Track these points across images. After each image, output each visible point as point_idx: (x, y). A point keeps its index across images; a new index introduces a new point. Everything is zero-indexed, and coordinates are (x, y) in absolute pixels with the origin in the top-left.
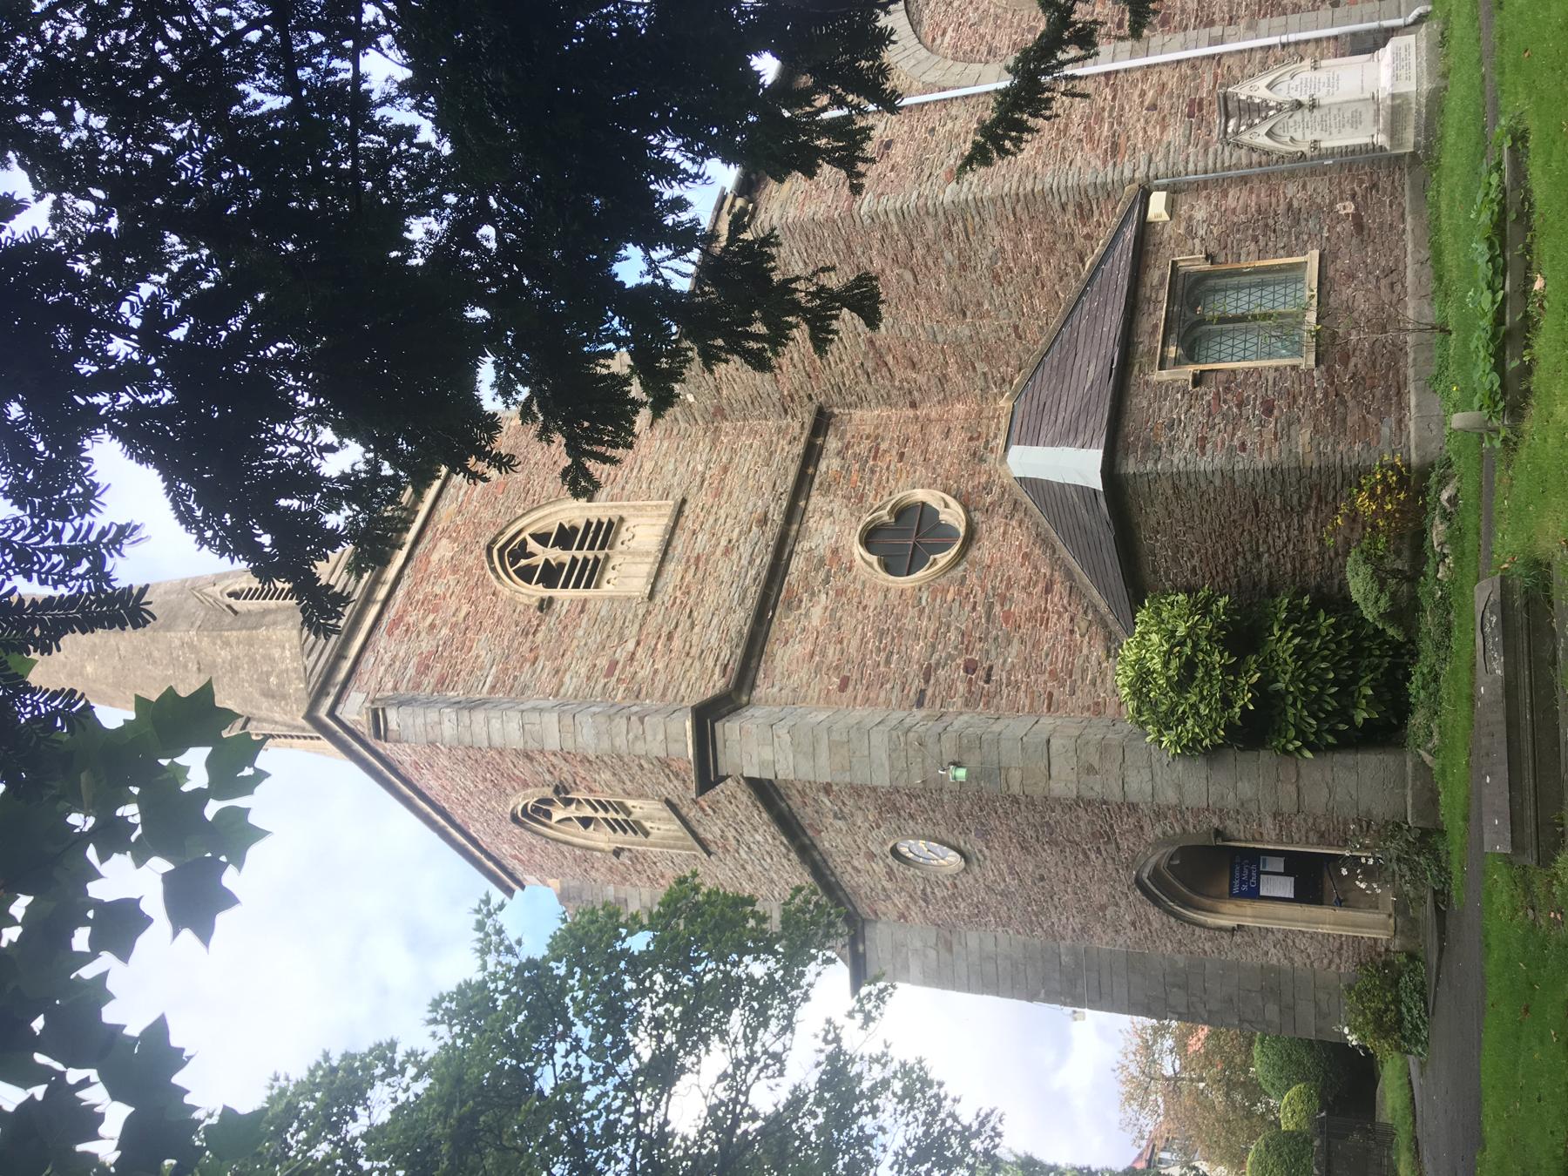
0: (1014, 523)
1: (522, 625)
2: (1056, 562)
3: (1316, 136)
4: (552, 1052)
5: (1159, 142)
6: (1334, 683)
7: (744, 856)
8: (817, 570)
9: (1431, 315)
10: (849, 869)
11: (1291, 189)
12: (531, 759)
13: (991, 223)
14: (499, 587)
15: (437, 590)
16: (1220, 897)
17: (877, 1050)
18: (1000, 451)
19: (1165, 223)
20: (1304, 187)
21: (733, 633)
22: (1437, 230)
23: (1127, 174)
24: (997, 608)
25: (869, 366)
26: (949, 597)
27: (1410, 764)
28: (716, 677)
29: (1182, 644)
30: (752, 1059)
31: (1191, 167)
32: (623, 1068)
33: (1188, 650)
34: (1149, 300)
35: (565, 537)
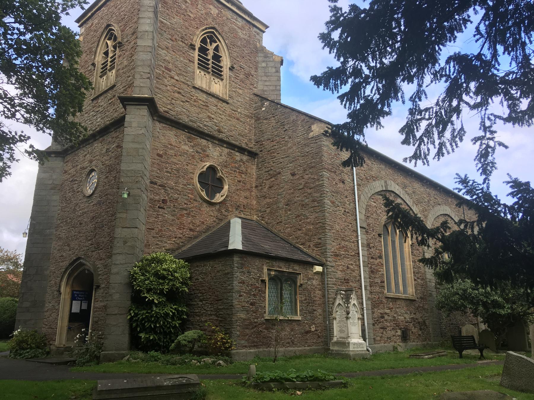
0: (215, 219)
1: (185, 37)
2: (201, 233)
3: (338, 319)
4: (20, 23)
5: (337, 269)
6: (155, 326)
7: (91, 114)
8: (201, 149)
9: (279, 355)
10: (85, 153)
11: (320, 311)
12: (133, 34)
13: (317, 215)
14: (200, 30)
15: (199, 6)
16: (72, 286)
17: (15, 156)
18: (239, 216)
19: (313, 271)
20: (320, 315)
21: (180, 116)
22: (305, 357)
23: (329, 259)
24: (185, 212)
25: (271, 172)
26: (189, 195)
27: (124, 352)
28: (164, 108)
29: (172, 275)
30: (13, 106)
31: (329, 279)
32: (11, 51)
33: (170, 277)
34: (289, 266)
35: (217, 58)
